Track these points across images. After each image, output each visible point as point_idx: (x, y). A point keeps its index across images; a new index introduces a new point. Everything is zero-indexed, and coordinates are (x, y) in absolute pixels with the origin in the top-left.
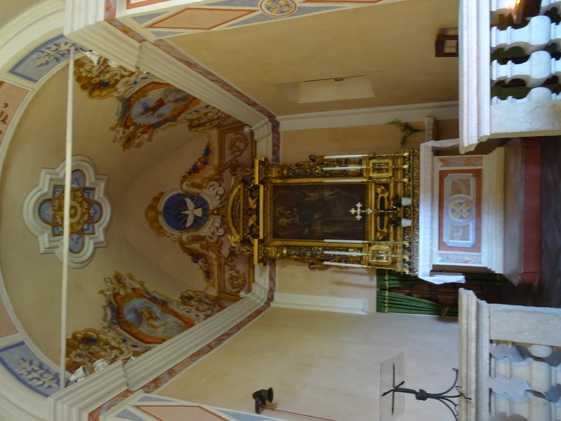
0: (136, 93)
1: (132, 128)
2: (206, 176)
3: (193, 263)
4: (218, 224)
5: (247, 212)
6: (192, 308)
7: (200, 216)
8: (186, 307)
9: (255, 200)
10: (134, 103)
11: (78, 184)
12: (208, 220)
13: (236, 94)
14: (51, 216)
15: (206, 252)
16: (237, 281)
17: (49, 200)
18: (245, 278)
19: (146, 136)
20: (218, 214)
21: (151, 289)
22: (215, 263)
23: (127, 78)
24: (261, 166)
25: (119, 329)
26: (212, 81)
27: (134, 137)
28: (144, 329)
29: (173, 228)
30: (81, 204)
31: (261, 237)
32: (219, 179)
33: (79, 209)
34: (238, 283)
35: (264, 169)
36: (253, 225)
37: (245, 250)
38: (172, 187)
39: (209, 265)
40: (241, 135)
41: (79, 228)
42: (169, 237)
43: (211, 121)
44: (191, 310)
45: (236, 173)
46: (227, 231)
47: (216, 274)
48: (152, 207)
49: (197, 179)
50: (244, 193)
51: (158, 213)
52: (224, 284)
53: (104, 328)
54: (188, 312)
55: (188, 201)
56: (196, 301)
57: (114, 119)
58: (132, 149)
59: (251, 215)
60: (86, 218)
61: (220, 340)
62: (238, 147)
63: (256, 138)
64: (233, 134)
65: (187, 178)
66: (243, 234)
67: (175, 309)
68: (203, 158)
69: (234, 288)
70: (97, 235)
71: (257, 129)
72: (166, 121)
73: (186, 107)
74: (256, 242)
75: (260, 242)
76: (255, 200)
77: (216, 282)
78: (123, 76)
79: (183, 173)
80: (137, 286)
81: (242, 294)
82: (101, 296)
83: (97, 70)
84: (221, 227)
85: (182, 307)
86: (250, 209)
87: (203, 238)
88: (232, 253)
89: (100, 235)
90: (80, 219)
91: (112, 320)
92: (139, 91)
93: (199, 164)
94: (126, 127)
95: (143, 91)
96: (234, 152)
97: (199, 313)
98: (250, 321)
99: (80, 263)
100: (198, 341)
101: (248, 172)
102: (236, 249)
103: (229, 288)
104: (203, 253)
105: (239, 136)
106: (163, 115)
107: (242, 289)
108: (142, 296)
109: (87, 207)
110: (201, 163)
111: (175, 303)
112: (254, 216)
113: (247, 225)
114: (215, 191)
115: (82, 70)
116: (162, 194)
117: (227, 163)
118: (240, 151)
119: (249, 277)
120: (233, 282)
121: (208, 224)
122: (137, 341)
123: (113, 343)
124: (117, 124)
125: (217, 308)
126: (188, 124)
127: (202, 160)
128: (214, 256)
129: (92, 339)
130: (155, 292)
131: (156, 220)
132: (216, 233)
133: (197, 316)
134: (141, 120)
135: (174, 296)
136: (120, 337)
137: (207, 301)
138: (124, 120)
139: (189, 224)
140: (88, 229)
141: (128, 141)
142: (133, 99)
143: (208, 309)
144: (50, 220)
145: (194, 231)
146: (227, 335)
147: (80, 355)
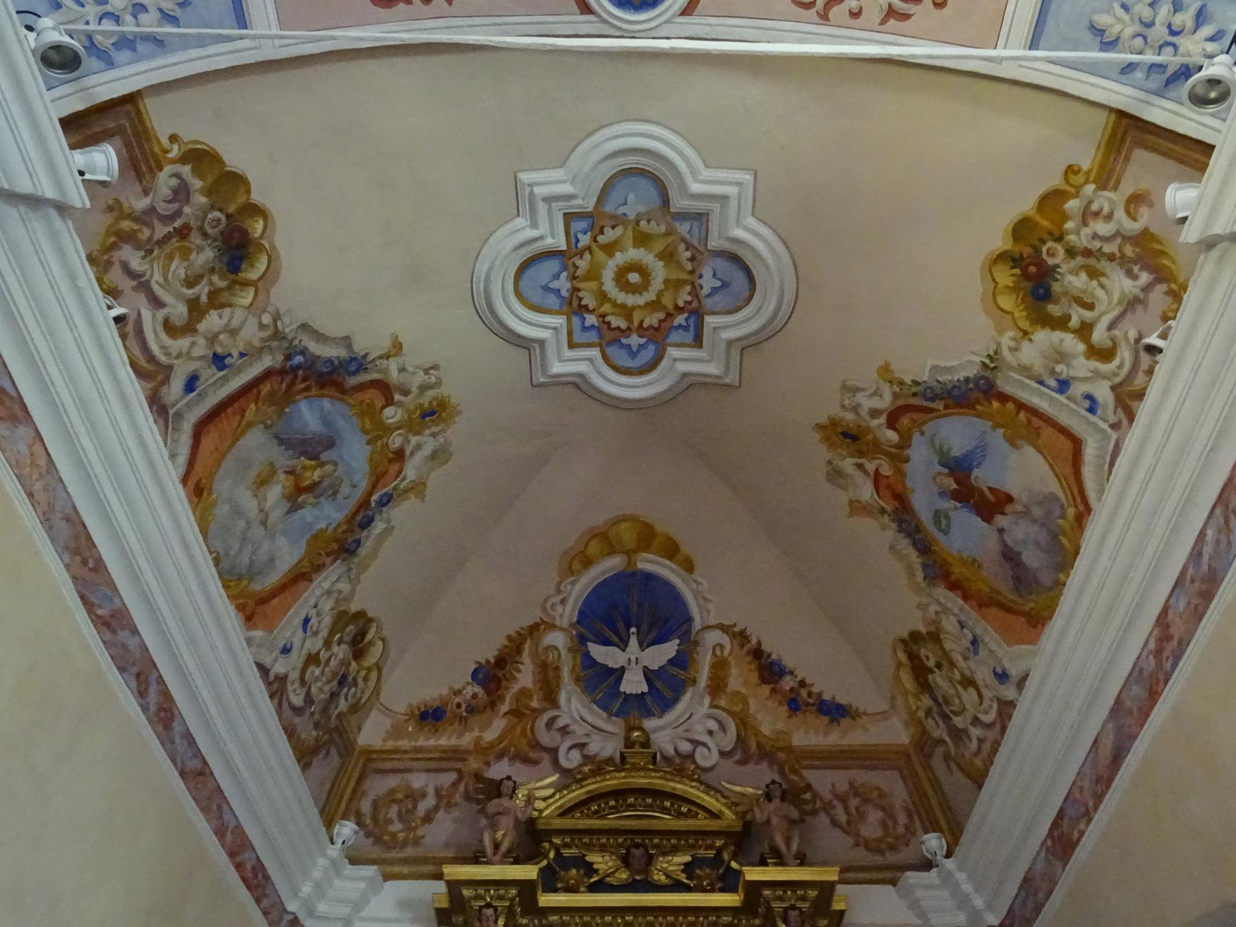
0: (1021, 406)
1: (892, 436)
2: (753, 707)
3: (474, 666)
4: (593, 748)
5: (637, 846)
6: (319, 643)
7: (622, 689)
8: (327, 620)
9: (683, 878)
10: (979, 415)
11: (715, 291)
12: (610, 714)
13: (1108, 742)
14: (622, 210)
15: (505, 708)
16: (400, 814)
17: (666, 201)
18: (404, 845)
19: (866, 491)
20: (629, 744)
21: (399, 513)
22: (466, 740)
23: (1081, 347)
24: (813, 894)
25: (267, 362)
26: (1162, 620)
27: (861, 454)
28: (256, 444)
29: (585, 603)
30: (654, 305)
31: (546, 900)
32: (748, 749)
33: (640, 300)
34: (390, 821)
35: (805, 906)
36: (590, 869)
37: (499, 834)
38: (710, 598)
39: (463, 720)
40: (907, 828)
41: (589, 301)
42: (559, 591)
43: (943, 709)
44: (315, 634)
45: (777, 801)
46: (570, 778)
47: (432, 742)
48: (647, 537)
49: (740, 677)
50: (703, 834)
51: (628, 553)
52: (394, 771)
53: (277, 317)
54: (306, 621)
55: (670, 649)
56: (345, 663)
57: (918, 367)
58: (823, 453)
59: (626, 861)
60: (616, 321)
61: (142, 674)
62: (861, 815)
63: (912, 877)
64: (905, 796)
65: (742, 646)
66: (560, 832)
67: (322, 582)
68: (810, 694)
69: (376, 805)
70: (568, 354)
71: (947, 877)
72: (924, 547)
73: (984, 602)
74: (529, 872)
75: (527, 889)
76: (683, 878)
77: (405, 744)
78: (1084, 331)
79: (756, 634)
80: (411, 471)
81: (346, 829)
82: (386, 345)
83: (1095, 236)
84: (585, 757)
85: (327, 605)
86: (650, 859)
87: (551, 699)
88: (495, 789)
89: (566, 363)
90: (615, 304)
91: (304, 352)
92: (1034, 412)
93: (788, 683)
94: (893, 420)
95: (1030, 425)
96: (843, 800)
97: (296, 659)
98: (220, 833)
99: (487, 280)
100: (149, 576)
101: (788, 841)
102: (505, 802)
103: (379, 786)
104: (502, 698)
105: (902, 819)
106: (946, 532)
107: (367, 835)
108: (377, 479)
109: (645, 325)
110: (792, 689)
111: (344, 586)
112: (624, 875)
113: (590, 847)
114: (704, 738)
115: (1090, 189)
116: (689, 567)
117: (801, 776)
118: (849, 822)
119: (406, 861)
120: (395, 801)
121: (597, 717)
122: (212, 400)
123: (213, 321)
124: (901, 383)
125: (309, 734)
126: (923, 630)
127: (804, 693)
128: (490, 735)
129: (241, 259)
130: (389, 530)
131: (611, 549)
132: (567, 743)
133: (286, 650)
134: (921, 465)
135: (373, 585)
136: (235, 354)
137: (343, 705)
138: (916, 401)
139: (597, 651)
140: (585, 329)
141: (847, 437)
142: (995, 404)
143: (309, 699)
144: (609, 208)
145: (573, 670)
146: (164, 715)
147: (181, 193)
